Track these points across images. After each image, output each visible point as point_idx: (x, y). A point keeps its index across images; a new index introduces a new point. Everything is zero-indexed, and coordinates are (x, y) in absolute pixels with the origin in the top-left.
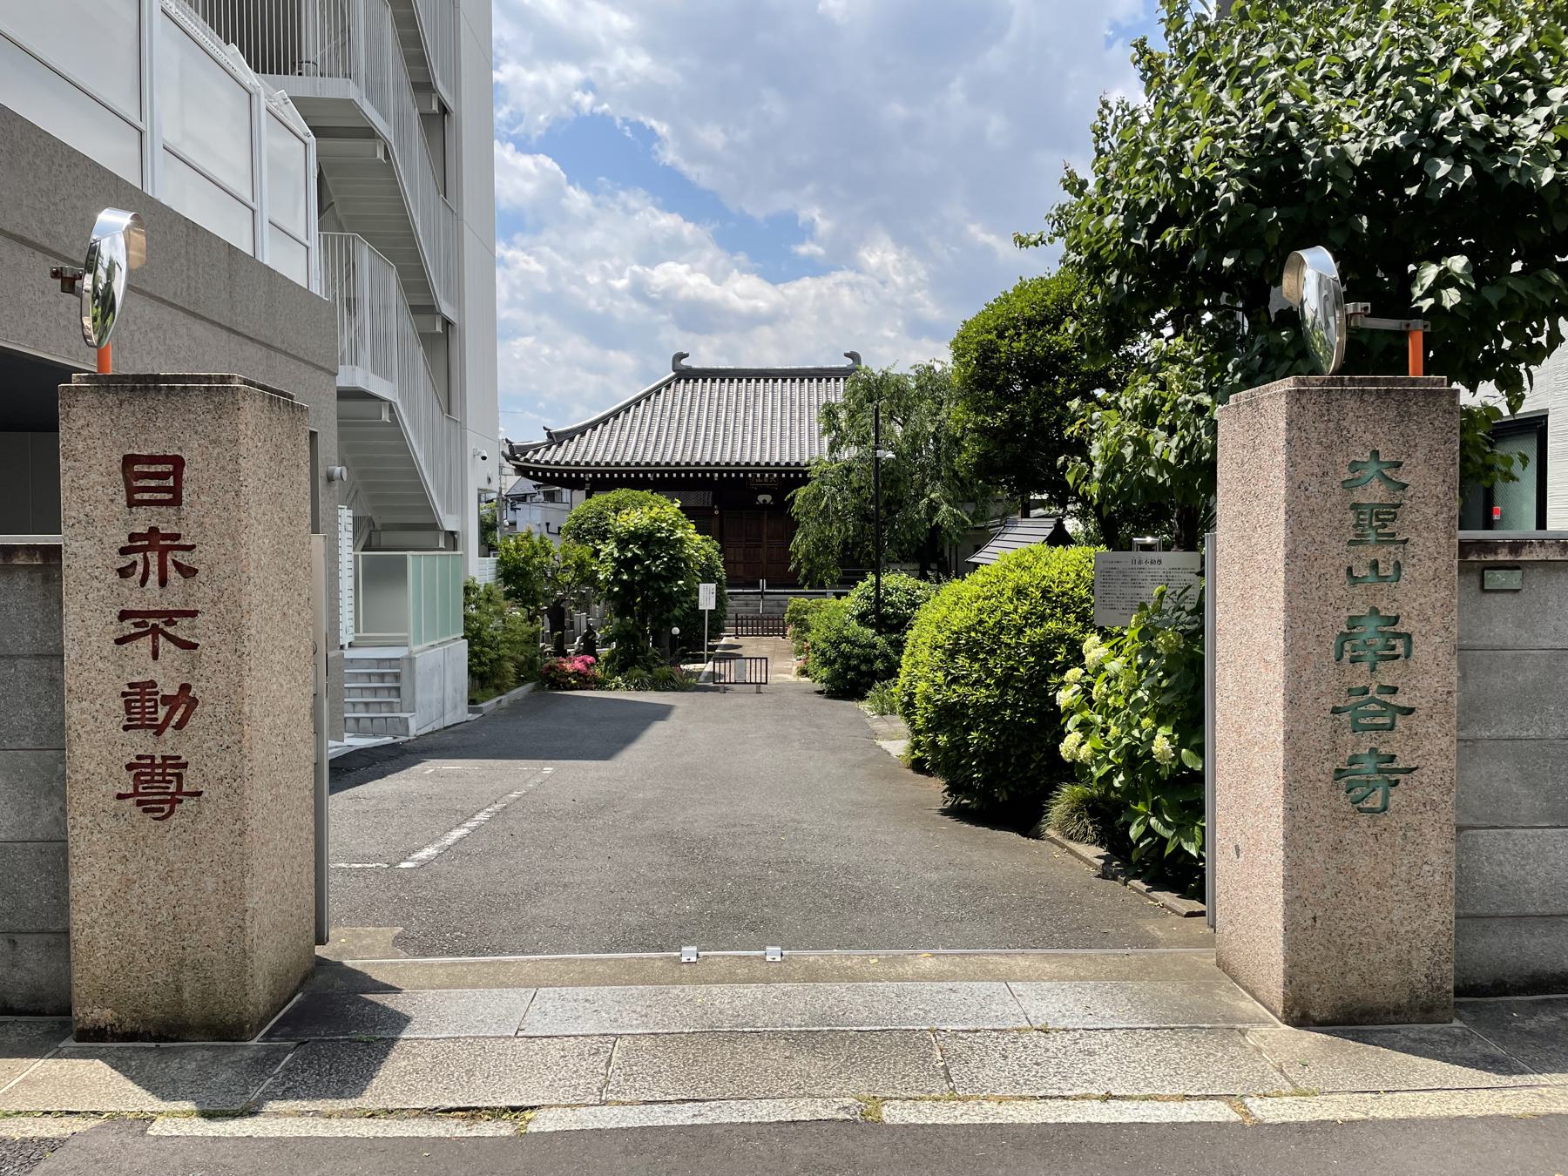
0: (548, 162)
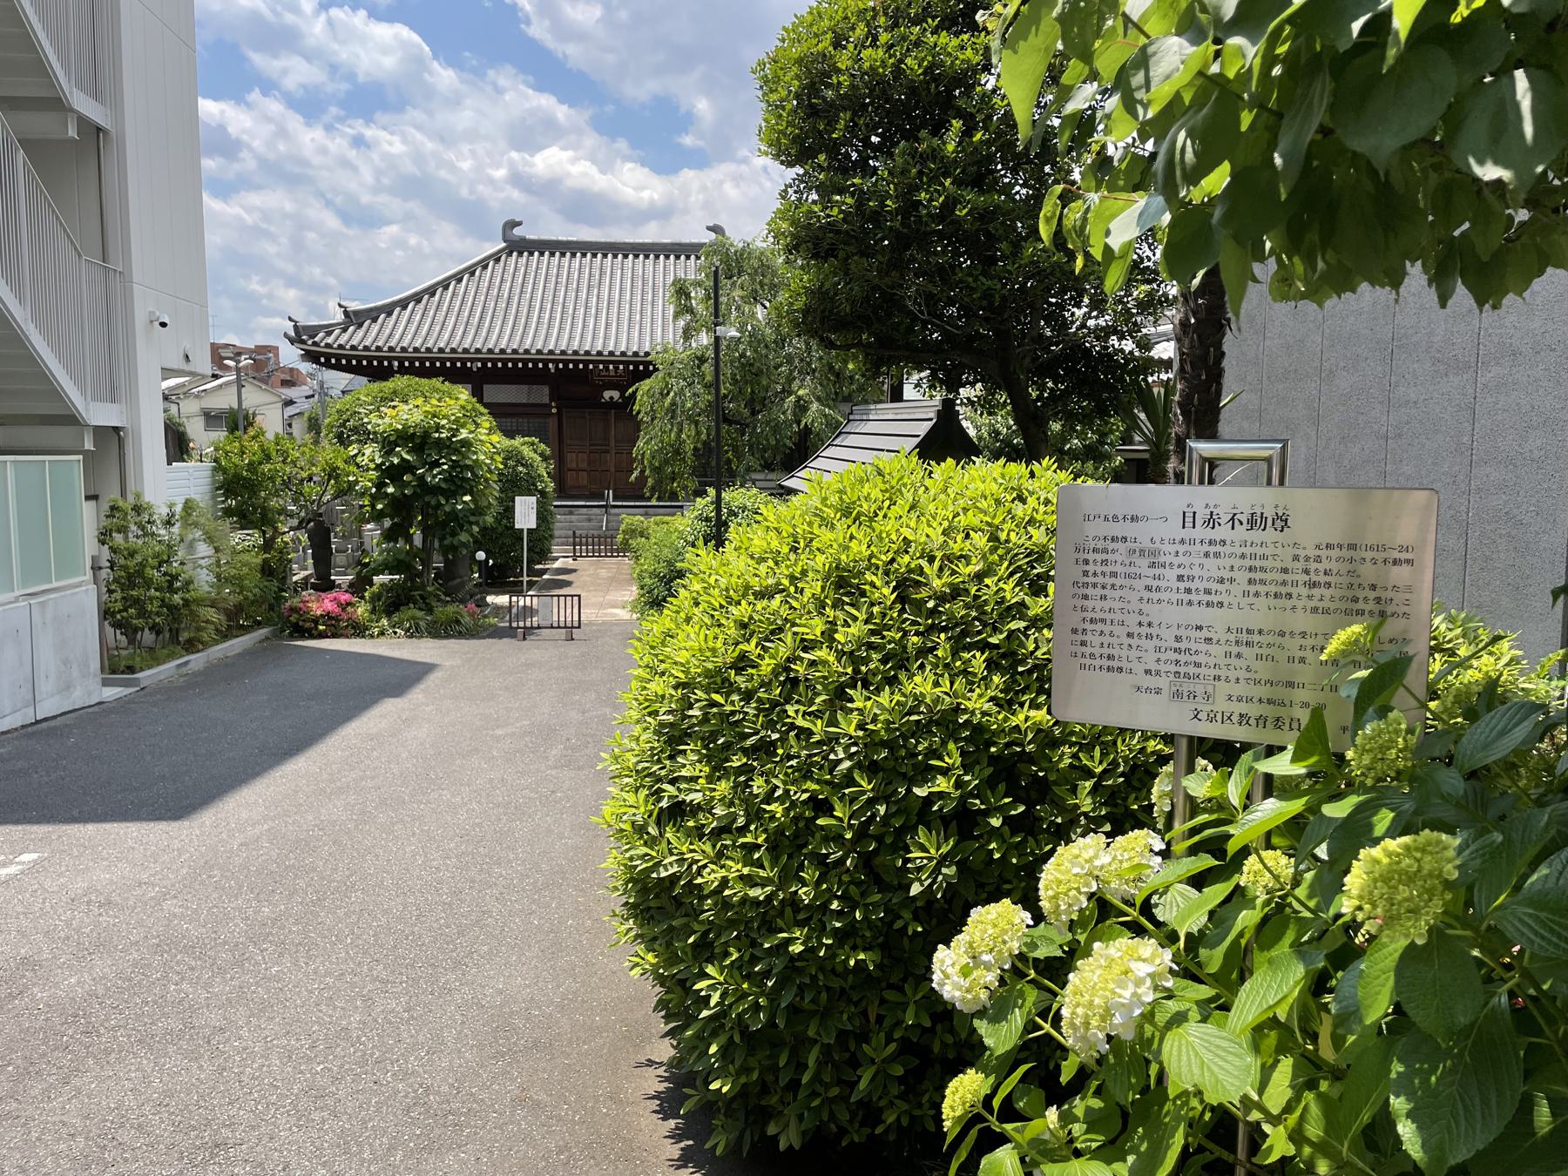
0: (405, 32)
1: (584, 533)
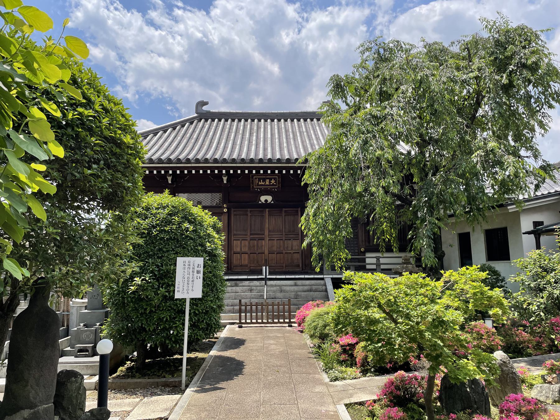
1: (247, 301)
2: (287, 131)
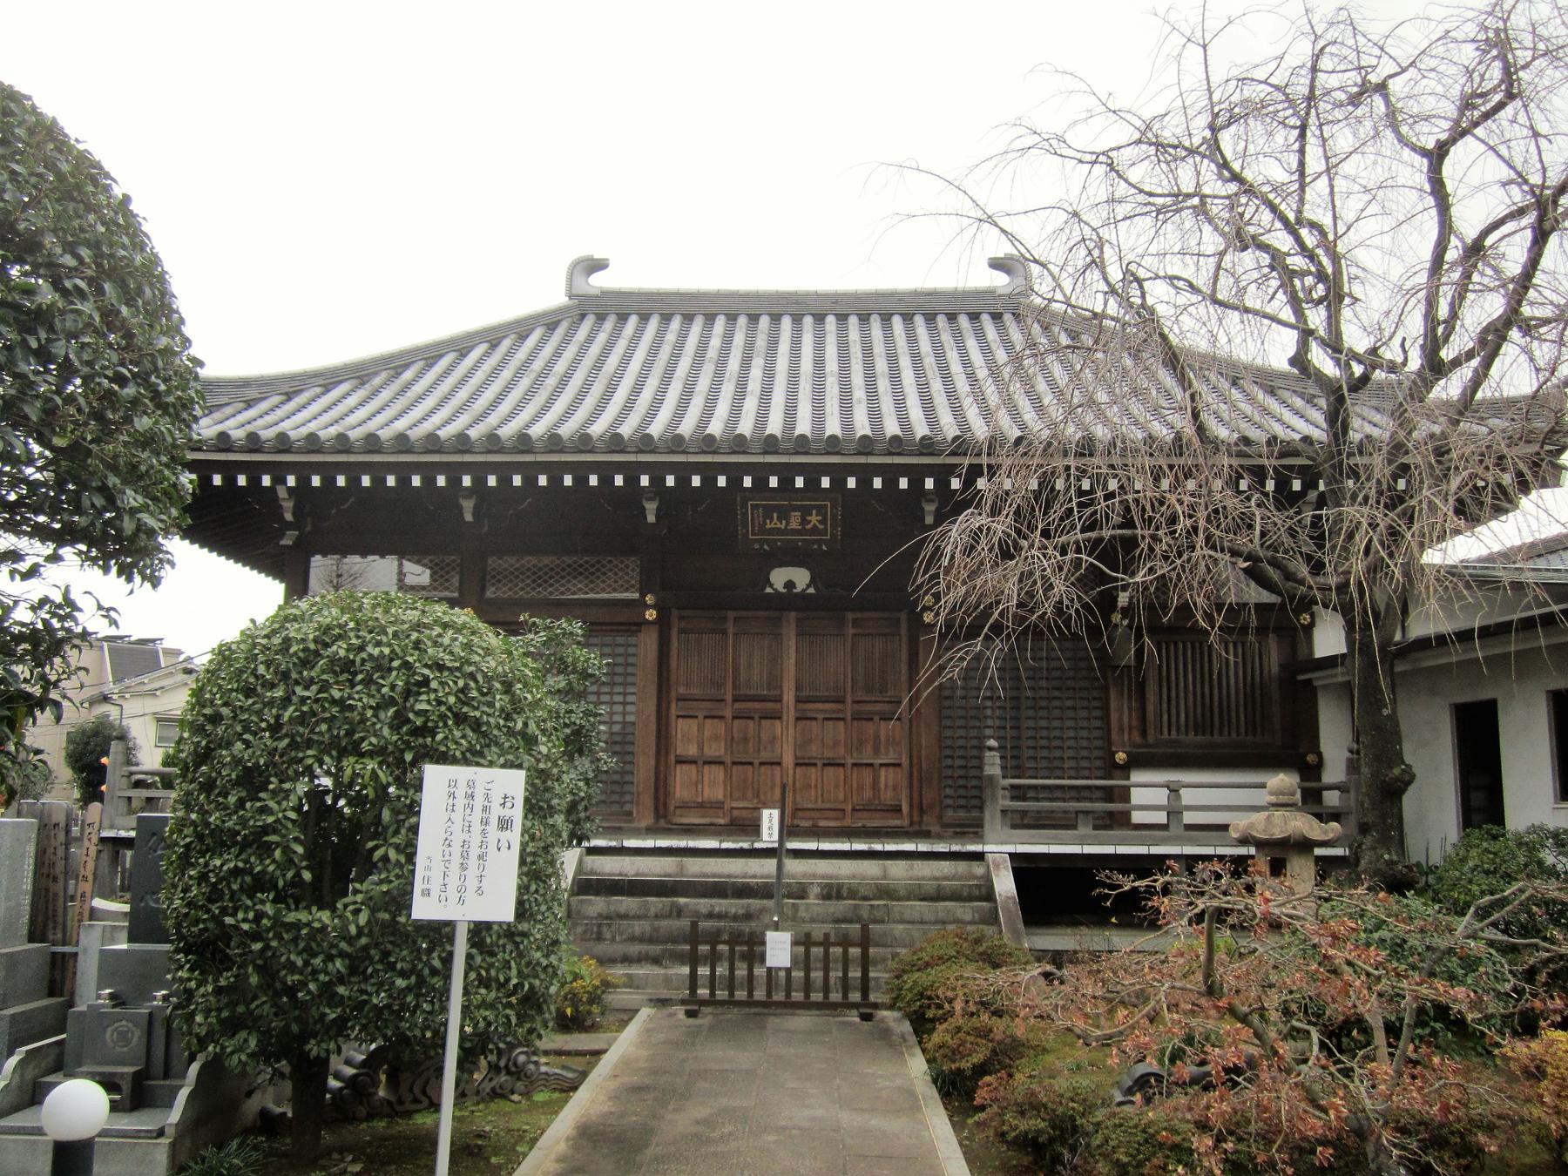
2: (868, 351)
